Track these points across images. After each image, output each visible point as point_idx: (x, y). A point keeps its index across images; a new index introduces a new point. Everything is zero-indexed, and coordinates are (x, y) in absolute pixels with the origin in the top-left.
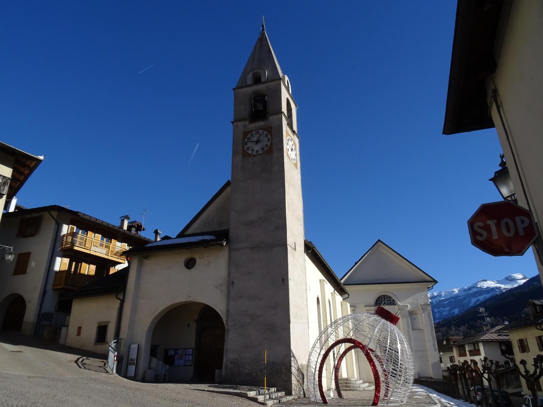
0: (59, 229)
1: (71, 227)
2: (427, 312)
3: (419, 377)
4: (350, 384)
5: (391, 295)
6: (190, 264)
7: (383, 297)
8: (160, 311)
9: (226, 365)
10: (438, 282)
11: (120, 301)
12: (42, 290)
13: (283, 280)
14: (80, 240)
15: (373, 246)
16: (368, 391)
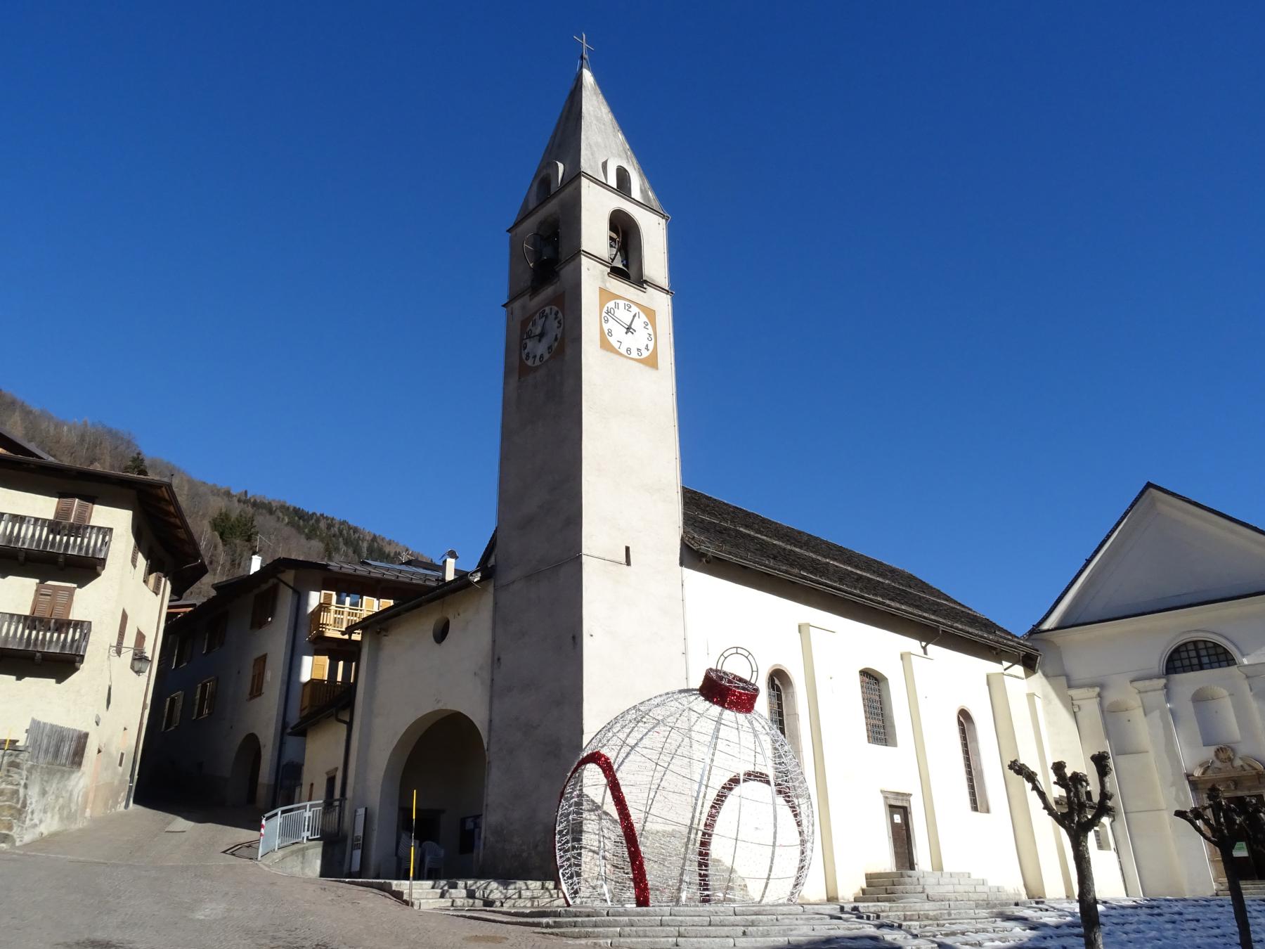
0: (301, 600)
6: (441, 634)
7: (1191, 647)
9: (485, 838)
11: (345, 725)
12: (280, 724)
13: (574, 638)
15: (1132, 506)
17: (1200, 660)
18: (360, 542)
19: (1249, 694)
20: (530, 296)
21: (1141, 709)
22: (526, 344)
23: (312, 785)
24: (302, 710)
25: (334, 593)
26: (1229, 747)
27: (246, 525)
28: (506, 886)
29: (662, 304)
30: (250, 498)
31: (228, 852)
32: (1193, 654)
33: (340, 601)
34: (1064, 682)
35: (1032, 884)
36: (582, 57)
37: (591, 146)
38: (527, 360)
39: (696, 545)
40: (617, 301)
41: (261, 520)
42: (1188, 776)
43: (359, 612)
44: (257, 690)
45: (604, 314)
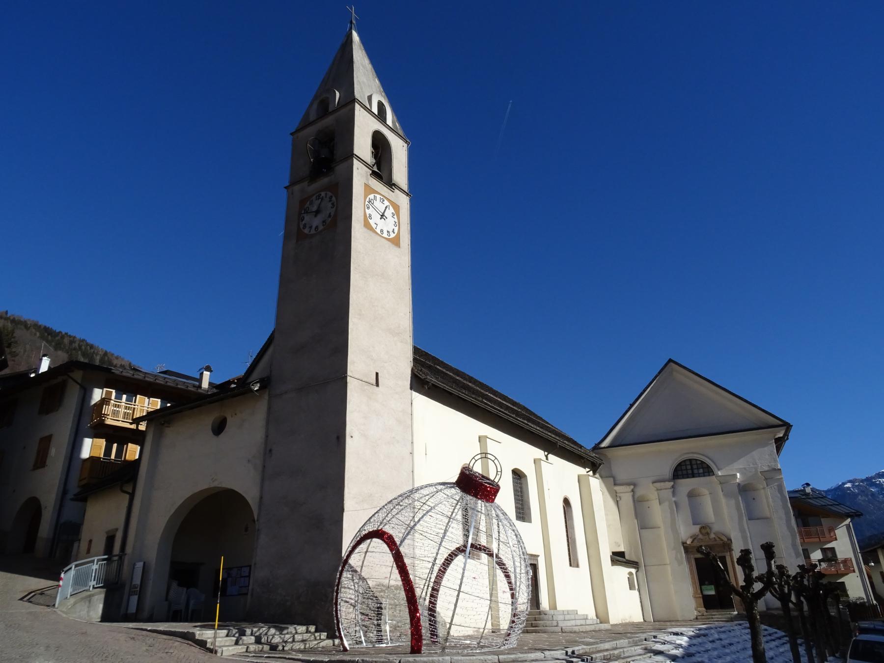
0: (86, 395)
1: (106, 391)
2: (776, 484)
3: (768, 609)
4: (543, 621)
5: (695, 455)
6: (219, 428)
7: (688, 463)
8: (176, 507)
10: (792, 426)
13: (338, 438)
14: (120, 410)
15: (660, 372)
16: (571, 632)
17: (693, 472)
18: (95, 355)
19: (721, 494)
20: (308, 183)
21: (658, 500)
22: (304, 217)
23: (91, 541)
24: (80, 480)
25: (114, 391)
26: (708, 526)
27: (7, 335)
28: (281, 630)
29: (404, 202)
30: (10, 316)
31: (25, 599)
32: (689, 467)
33: (119, 397)
34: (612, 482)
35: (601, 614)
36: (351, 22)
37: (360, 83)
38: (304, 228)
39: (423, 375)
40: (376, 195)
41: (19, 333)
42: (684, 543)
43: (132, 406)
44: (41, 461)
45: (367, 203)
